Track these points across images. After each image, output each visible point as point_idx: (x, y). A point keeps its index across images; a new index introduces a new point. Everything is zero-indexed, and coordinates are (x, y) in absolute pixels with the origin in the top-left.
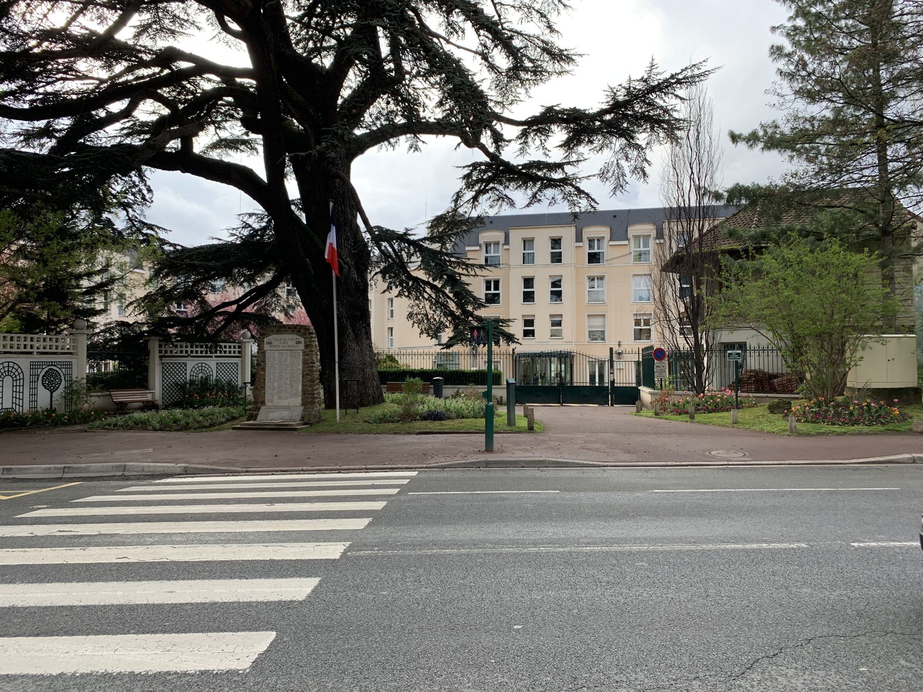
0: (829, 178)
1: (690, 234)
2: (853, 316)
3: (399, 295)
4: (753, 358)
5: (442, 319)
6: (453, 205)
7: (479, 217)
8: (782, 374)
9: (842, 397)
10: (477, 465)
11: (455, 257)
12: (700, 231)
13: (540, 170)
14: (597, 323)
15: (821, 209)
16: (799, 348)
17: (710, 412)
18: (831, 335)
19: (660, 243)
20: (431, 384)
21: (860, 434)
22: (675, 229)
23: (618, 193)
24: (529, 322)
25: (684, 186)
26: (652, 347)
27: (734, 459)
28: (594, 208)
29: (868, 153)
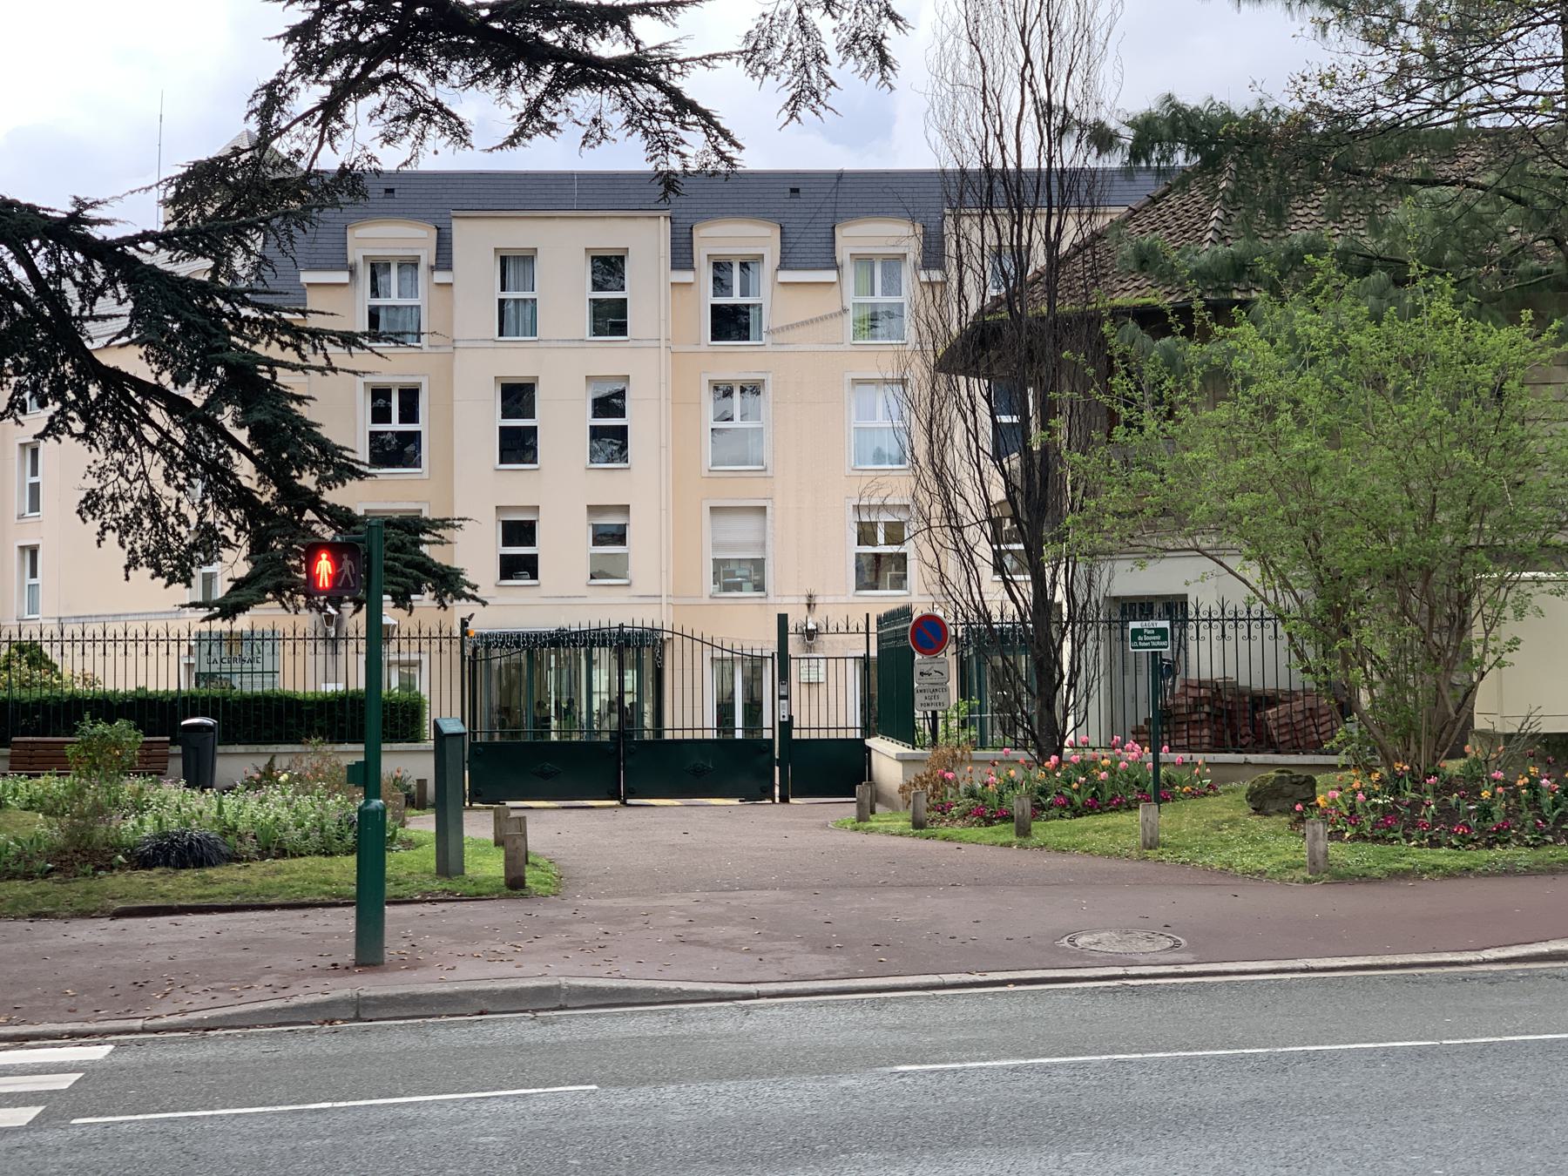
0: (1429, 94)
1: (1021, 256)
2: (1490, 515)
3: (53, 429)
4: (1204, 645)
5: (210, 518)
6: (254, 126)
7: (344, 172)
8: (1291, 692)
9: (1462, 762)
10: (325, 1014)
11: (255, 305)
12: (1051, 245)
13: (550, 24)
14: (740, 538)
15: (1402, 187)
16: (1337, 613)
17: (1077, 814)
18: (1427, 573)
19: (931, 284)
20: (173, 742)
21: (1509, 871)
22: (975, 235)
23: (804, 112)
24: (519, 531)
25: (1004, 101)
26: (906, 612)
27: (1143, 959)
28: (729, 160)
29: (1535, 26)
